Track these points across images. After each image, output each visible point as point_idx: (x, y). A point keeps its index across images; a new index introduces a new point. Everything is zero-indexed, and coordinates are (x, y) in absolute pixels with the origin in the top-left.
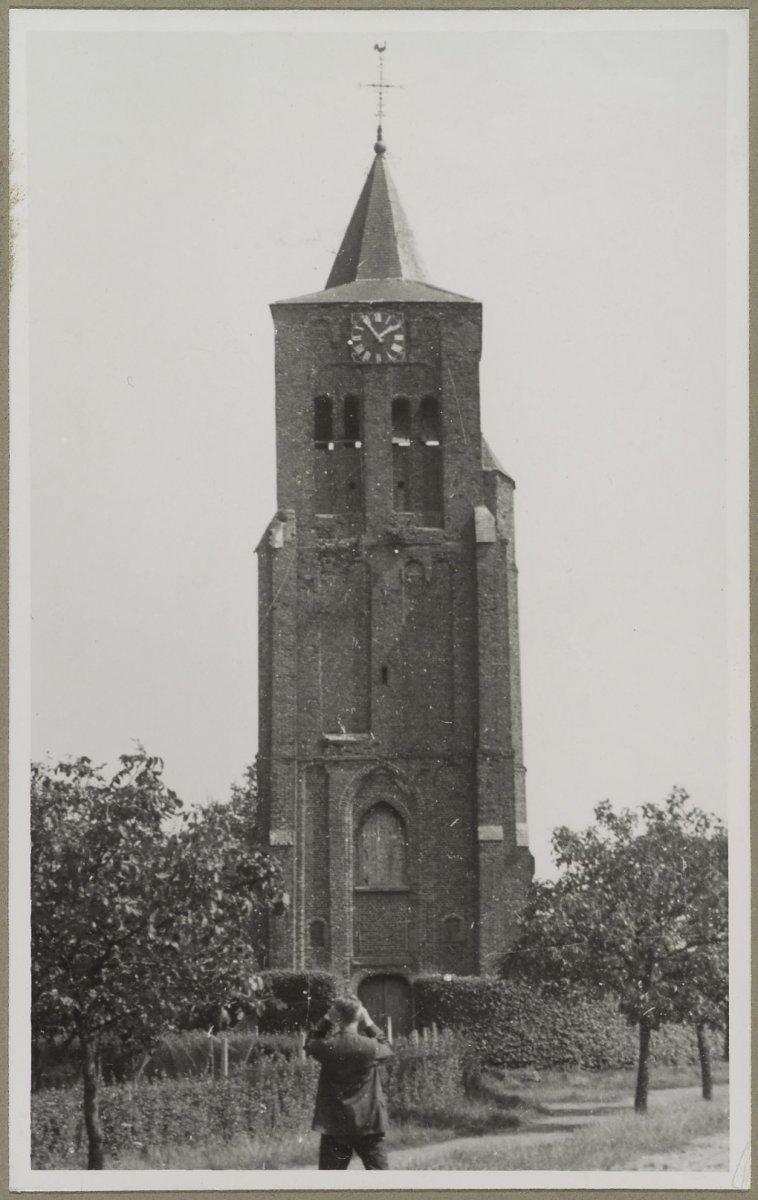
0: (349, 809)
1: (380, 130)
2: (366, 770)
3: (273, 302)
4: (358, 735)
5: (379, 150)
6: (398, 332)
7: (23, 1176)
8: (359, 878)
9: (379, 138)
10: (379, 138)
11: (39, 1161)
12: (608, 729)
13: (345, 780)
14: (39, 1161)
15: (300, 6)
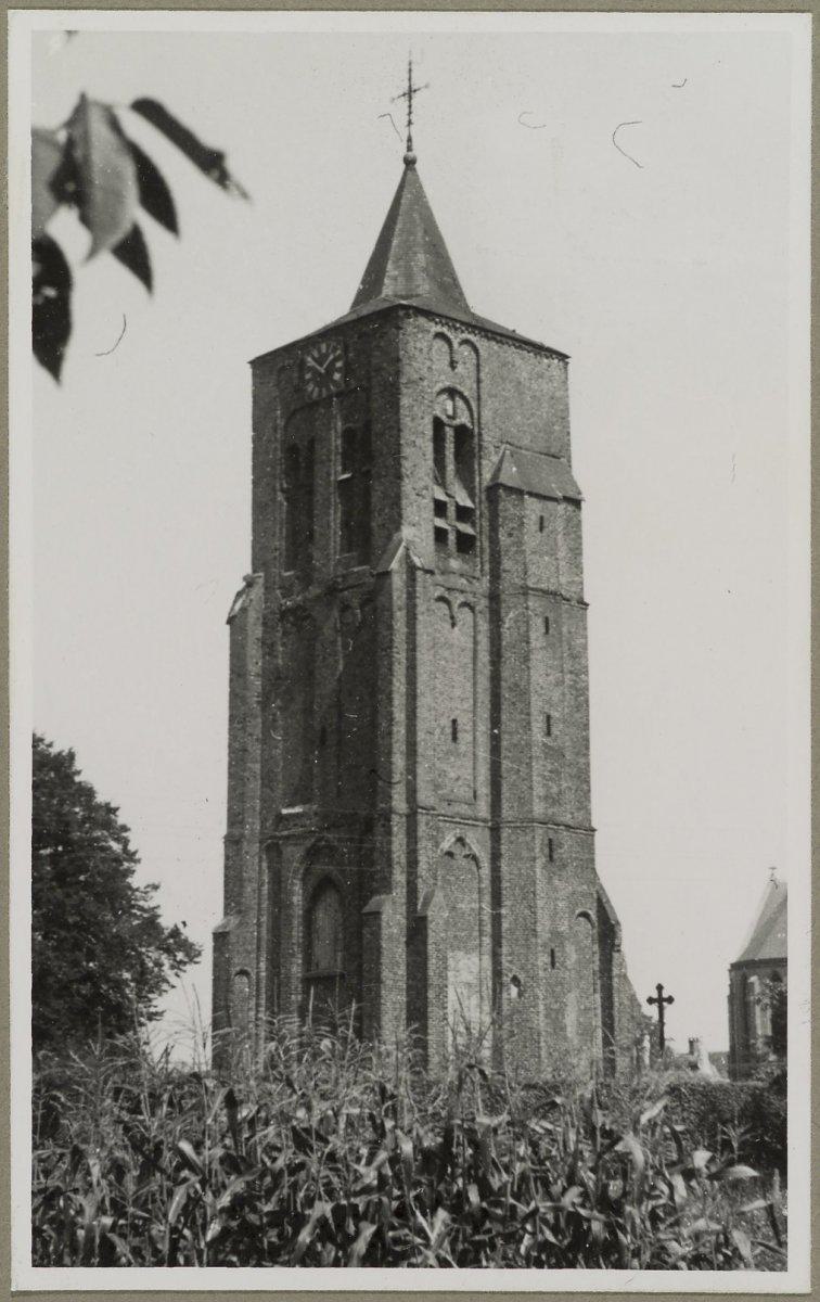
0: (298, 888)
1: (409, 140)
2: (309, 843)
3: (252, 357)
4: (307, 806)
5: (410, 163)
6: (336, 359)
7: (26, 1275)
8: (308, 961)
9: (409, 149)
10: (409, 149)
11: (42, 1258)
12: (687, 860)
13: (294, 854)
14: (42, 1258)
15: (553, 7)
